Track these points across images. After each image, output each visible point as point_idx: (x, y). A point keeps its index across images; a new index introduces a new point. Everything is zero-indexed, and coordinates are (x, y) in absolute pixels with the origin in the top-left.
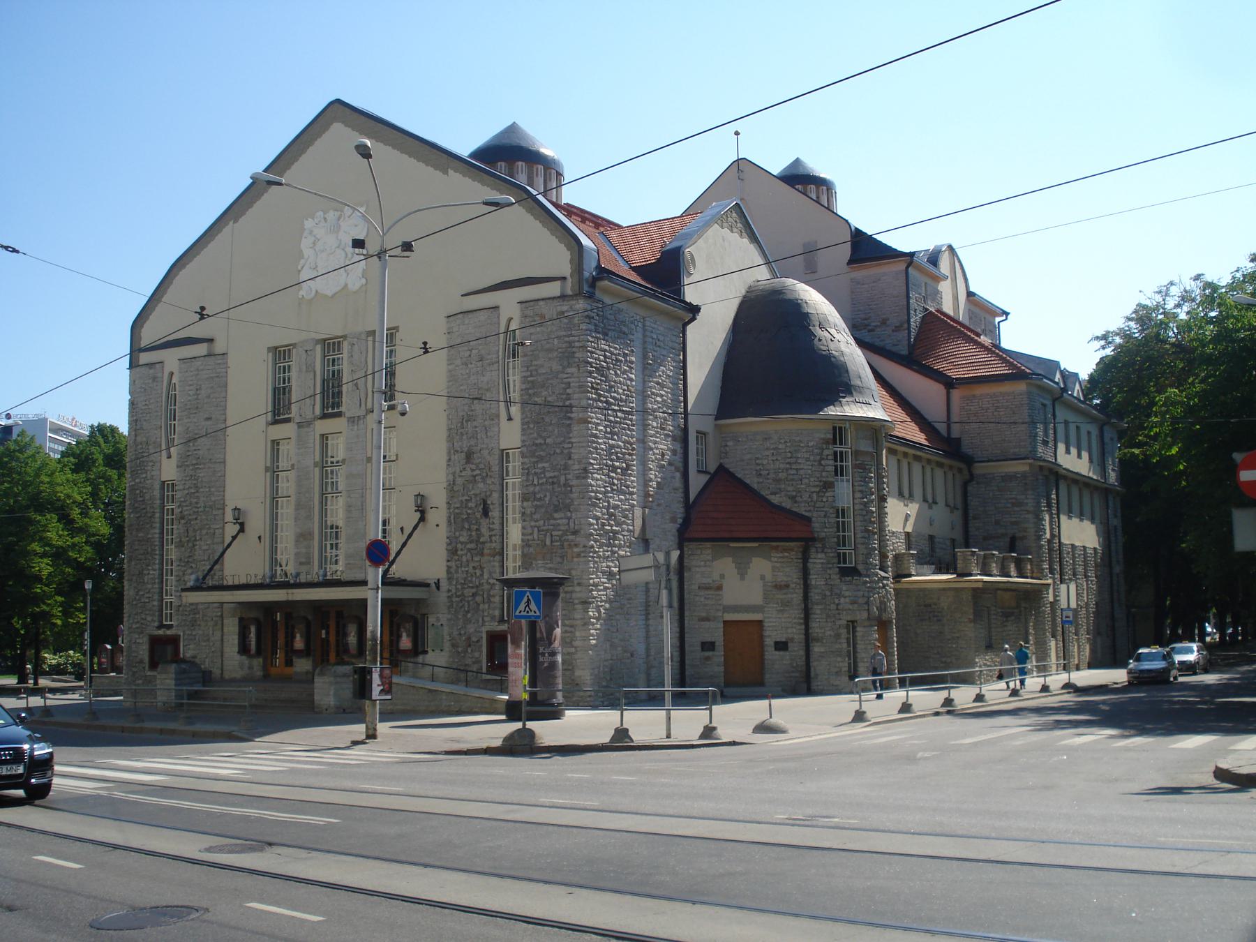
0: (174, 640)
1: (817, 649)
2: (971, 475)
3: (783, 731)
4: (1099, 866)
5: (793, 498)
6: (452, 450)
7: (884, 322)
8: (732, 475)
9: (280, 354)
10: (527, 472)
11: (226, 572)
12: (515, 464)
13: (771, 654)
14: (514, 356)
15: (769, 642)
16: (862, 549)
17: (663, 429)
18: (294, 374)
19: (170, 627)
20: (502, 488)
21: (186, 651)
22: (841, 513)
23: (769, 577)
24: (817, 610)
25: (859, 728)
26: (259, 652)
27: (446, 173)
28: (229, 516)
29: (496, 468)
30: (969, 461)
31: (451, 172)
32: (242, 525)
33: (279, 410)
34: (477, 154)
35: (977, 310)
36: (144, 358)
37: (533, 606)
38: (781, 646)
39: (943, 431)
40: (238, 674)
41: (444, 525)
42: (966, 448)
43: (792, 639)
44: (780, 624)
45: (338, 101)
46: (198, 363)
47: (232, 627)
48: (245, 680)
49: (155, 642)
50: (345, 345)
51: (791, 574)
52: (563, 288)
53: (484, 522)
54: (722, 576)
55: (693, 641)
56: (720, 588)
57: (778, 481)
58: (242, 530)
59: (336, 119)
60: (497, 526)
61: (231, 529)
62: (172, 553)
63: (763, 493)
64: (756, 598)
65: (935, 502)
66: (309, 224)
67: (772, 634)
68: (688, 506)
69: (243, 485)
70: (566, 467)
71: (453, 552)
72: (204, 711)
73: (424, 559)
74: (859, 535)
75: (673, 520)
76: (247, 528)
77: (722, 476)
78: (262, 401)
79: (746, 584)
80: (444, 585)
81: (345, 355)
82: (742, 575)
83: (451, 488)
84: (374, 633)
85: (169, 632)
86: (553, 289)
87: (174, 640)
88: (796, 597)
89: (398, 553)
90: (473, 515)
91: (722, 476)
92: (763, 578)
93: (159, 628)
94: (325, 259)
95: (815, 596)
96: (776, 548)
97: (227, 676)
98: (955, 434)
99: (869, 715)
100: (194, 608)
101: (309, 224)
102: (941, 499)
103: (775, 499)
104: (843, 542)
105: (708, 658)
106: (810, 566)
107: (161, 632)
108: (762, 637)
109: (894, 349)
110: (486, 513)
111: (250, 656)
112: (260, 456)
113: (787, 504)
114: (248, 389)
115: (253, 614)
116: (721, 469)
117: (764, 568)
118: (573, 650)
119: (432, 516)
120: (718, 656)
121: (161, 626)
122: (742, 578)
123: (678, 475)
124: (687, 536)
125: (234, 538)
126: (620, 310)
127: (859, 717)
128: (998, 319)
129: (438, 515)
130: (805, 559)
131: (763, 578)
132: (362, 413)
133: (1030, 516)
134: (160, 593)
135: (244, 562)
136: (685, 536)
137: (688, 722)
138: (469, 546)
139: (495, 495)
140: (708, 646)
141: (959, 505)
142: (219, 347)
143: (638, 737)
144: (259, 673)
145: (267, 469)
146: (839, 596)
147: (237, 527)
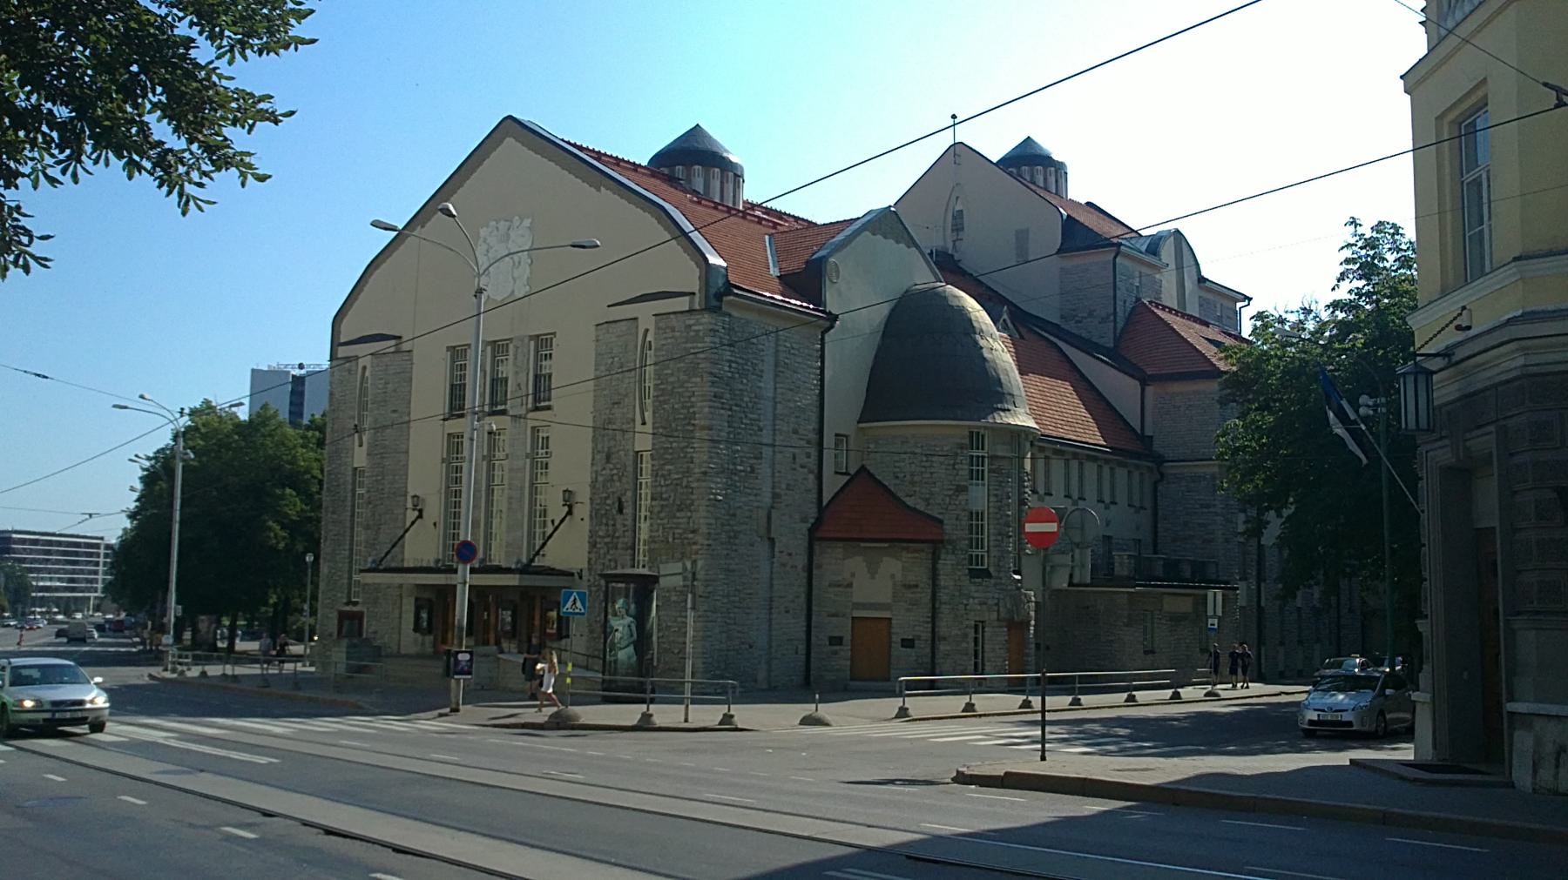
0: (359, 617)
1: (943, 647)
2: (1162, 475)
3: (827, 725)
4: (210, 793)
5: (927, 500)
6: (595, 451)
7: (1091, 314)
8: (871, 475)
10: (655, 474)
11: (407, 555)
12: (647, 465)
13: (898, 650)
15: (896, 639)
16: (994, 552)
18: (469, 372)
19: (356, 604)
20: (636, 486)
21: (368, 627)
22: (979, 516)
23: (899, 577)
24: (944, 609)
25: (898, 723)
26: (429, 630)
29: (630, 469)
30: (1160, 460)
32: (421, 511)
33: (456, 407)
34: (661, 159)
35: (1210, 296)
36: (342, 352)
37: (579, 604)
38: (908, 643)
39: (1136, 424)
40: (413, 650)
41: (587, 519)
42: (1157, 446)
43: (919, 638)
44: (908, 621)
45: (510, 117)
46: (386, 359)
47: (409, 606)
48: (419, 656)
49: (343, 616)
51: (920, 575)
52: (691, 302)
53: (619, 518)
54: (853, 575)
55: (820, 638)
56: (850, 585)
57: (913, 483)
58: (420, 516)
59: (507, 135)
60: (629, 522)
62: (361, 535)
63: (900, 494)
64: (885, 597)
66: (483, 232)
67: (900, 632)
68: (821, 509)
69: (424, 475)
70: (688, 470)
71: (593, 545)
72: (367, 681)
73: (569, 550)
75: (804, 520)
77: (862, 477)
79: (874, 582)
80: (585, 573)
81: (511, 357)
82: (873, 573)
83: (593, 485)
84: (461, 621)
85: (355, 609)
86: (682, 304)
87: (359, 617)
88: (926, 598)
90: (611, 508)
91: (862, 477)
93: (348, 604)
94: (505, 264)
95: (943, 596)
96: (907, 549)
97: (403, 652)
98: (1148, 432)
99: (911, 712)
100: (377, 588)
101: (483, 232)
102: (1122, 497)
103: (910, 502)
104: (979, 544)
105: (836, 653)
106: (939, 566)
107: (347, 608)
108: (890, 633)
109: (1101, 341)
110: (620, 511)
111: (423, 634)
113: (921, 507)
115: (426, 595)
116: (863, 469)
117: (893, 567)
120: (845, 650)
121: (349, 603)
122: (873, 577)
123: (811, 477)
124: (819, 535)
126: (748, 322)
127: (903, 713)
128: (1239, 305)
129: (583, 510)
130: (935, 558)
131: (893, 576)
132: (523, 412)
133: (1219, 519)
134: (339, 573)
136: (816, 535)
137: (710, 714)
139: (629, 494)
140: (837, 641)
141: (1148, 504)
143: (658, 720)
144: (430, 650)
145: (443, 461)
146: (969, 597)
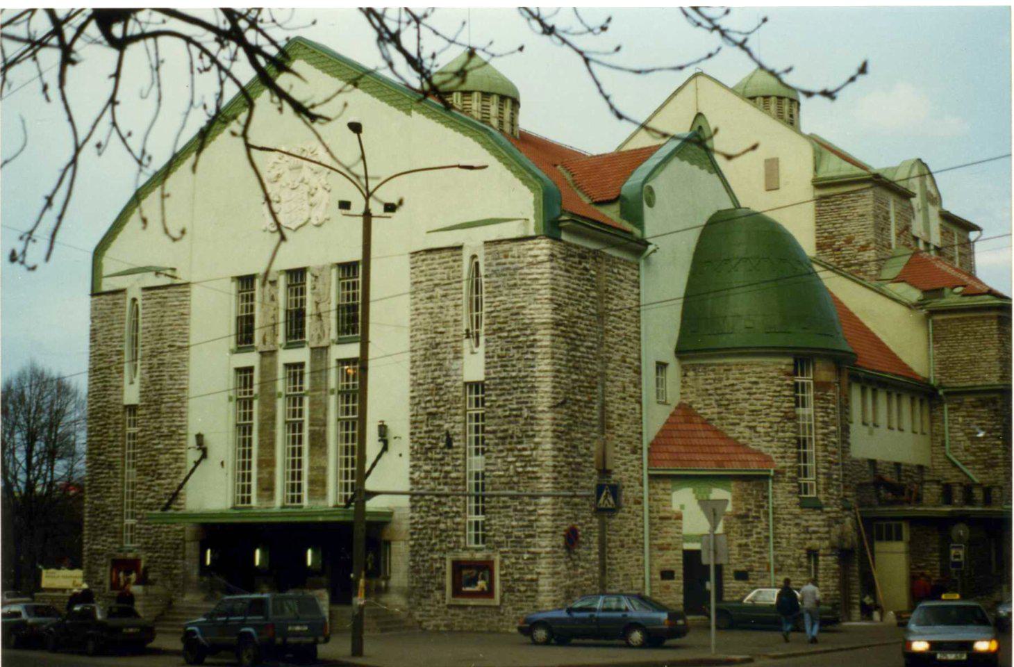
9: (246, 282)
14: (553, 289)
17: (625, 362)
27: (409, 113)
28: (192, 441)
31: (414, 112)
33: (245, 334)
37: (611, 500)
50: (309, 277)
54: (682, 507)
58: (204, 456)
61: (193, 455)
65: (876, 425)
74: (821, 465)
76: (210, 454)
78: (228, 327)
89: (374, 465)
105: (667, 587)
112: (227, 381)
114: (210, 316)
118: (535, 577)
119: (392, 444)
125: (197, 463)
135: (211, 492)
147: (199, 454)
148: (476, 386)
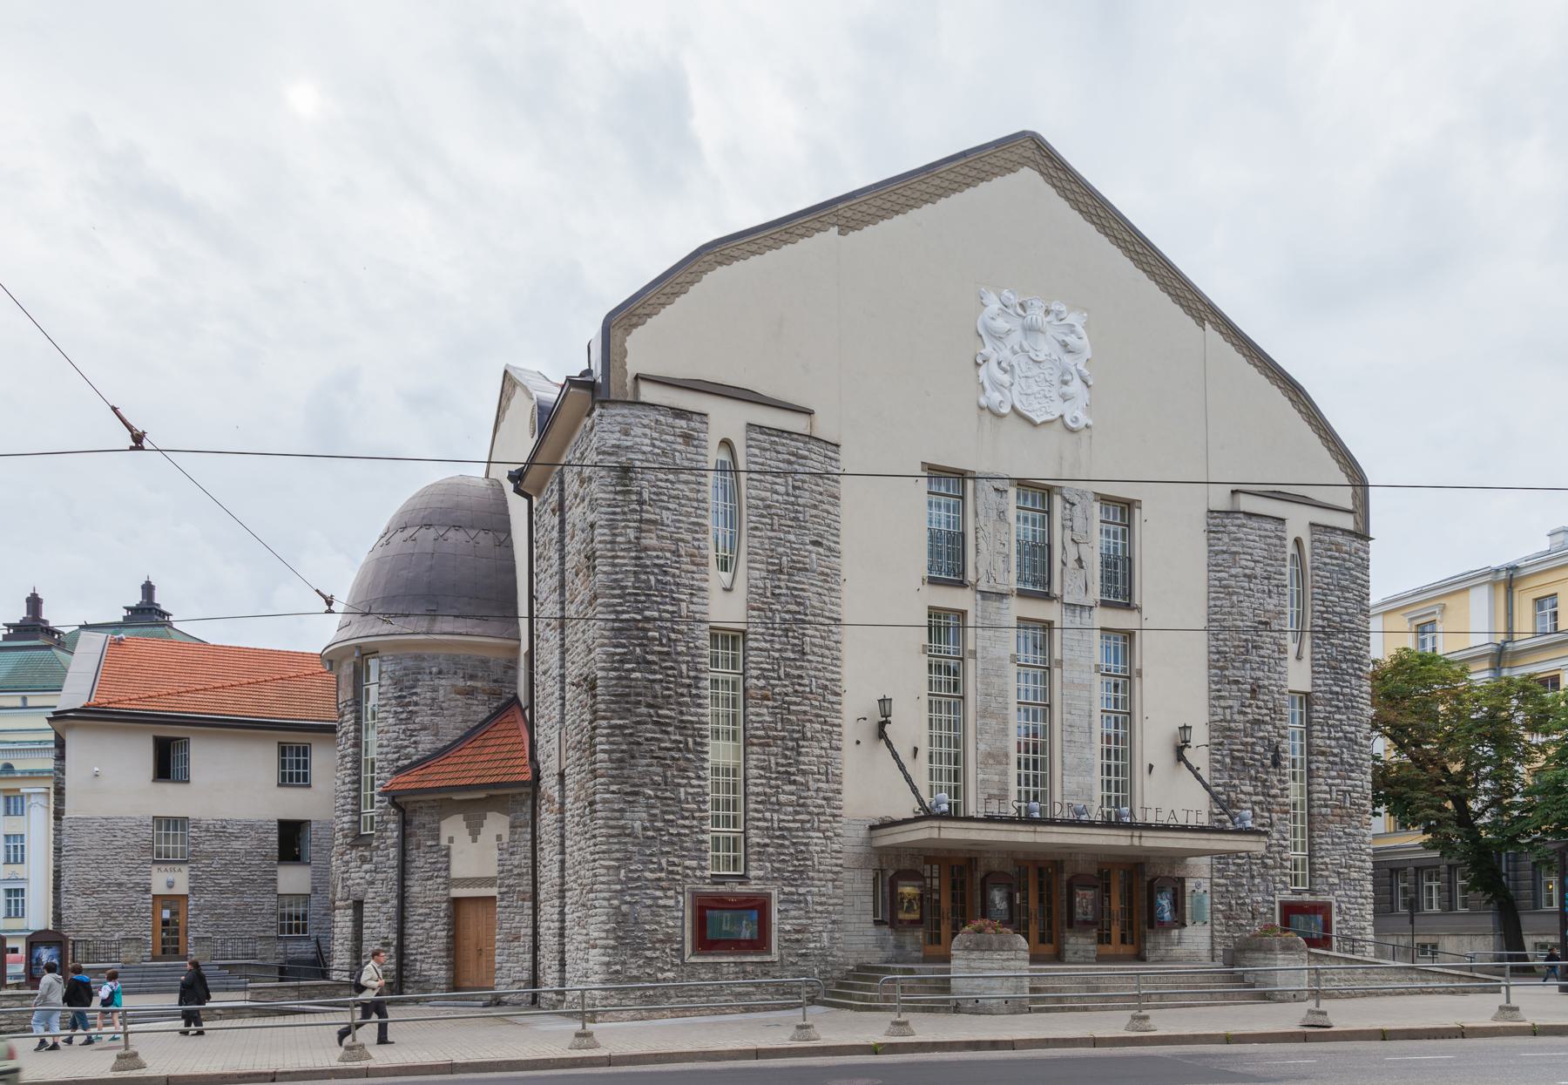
69: (876, 657)
82: (474, 834)
92: (499, 838)
110: (1276, 764)
138: (1254, 798)
142: (824, 430)
148: (1307, 699)
